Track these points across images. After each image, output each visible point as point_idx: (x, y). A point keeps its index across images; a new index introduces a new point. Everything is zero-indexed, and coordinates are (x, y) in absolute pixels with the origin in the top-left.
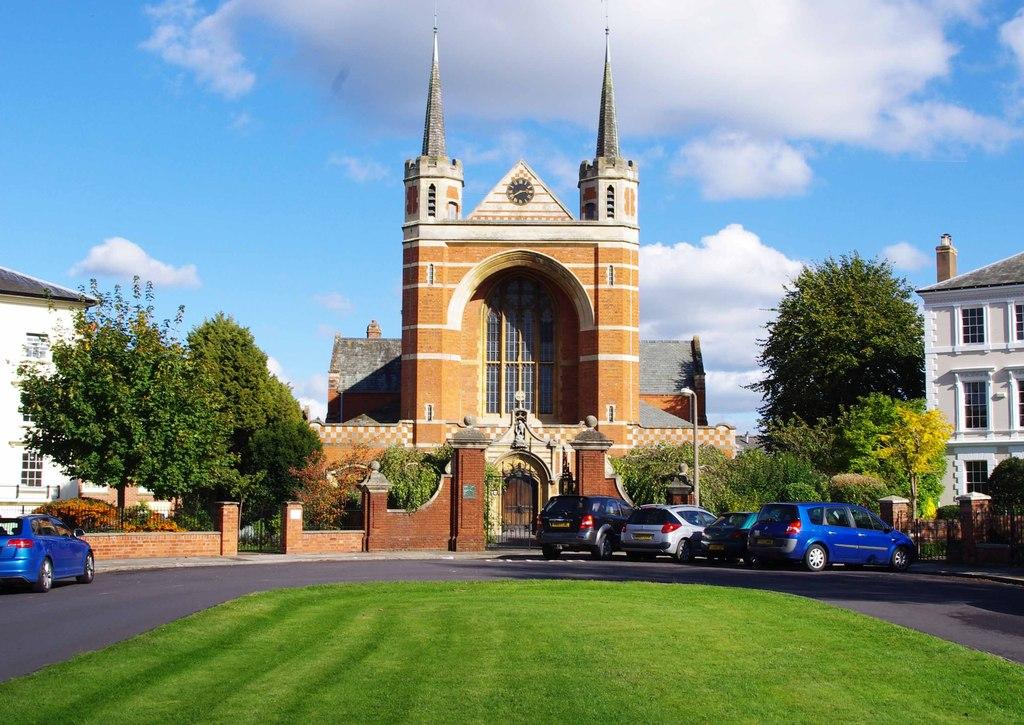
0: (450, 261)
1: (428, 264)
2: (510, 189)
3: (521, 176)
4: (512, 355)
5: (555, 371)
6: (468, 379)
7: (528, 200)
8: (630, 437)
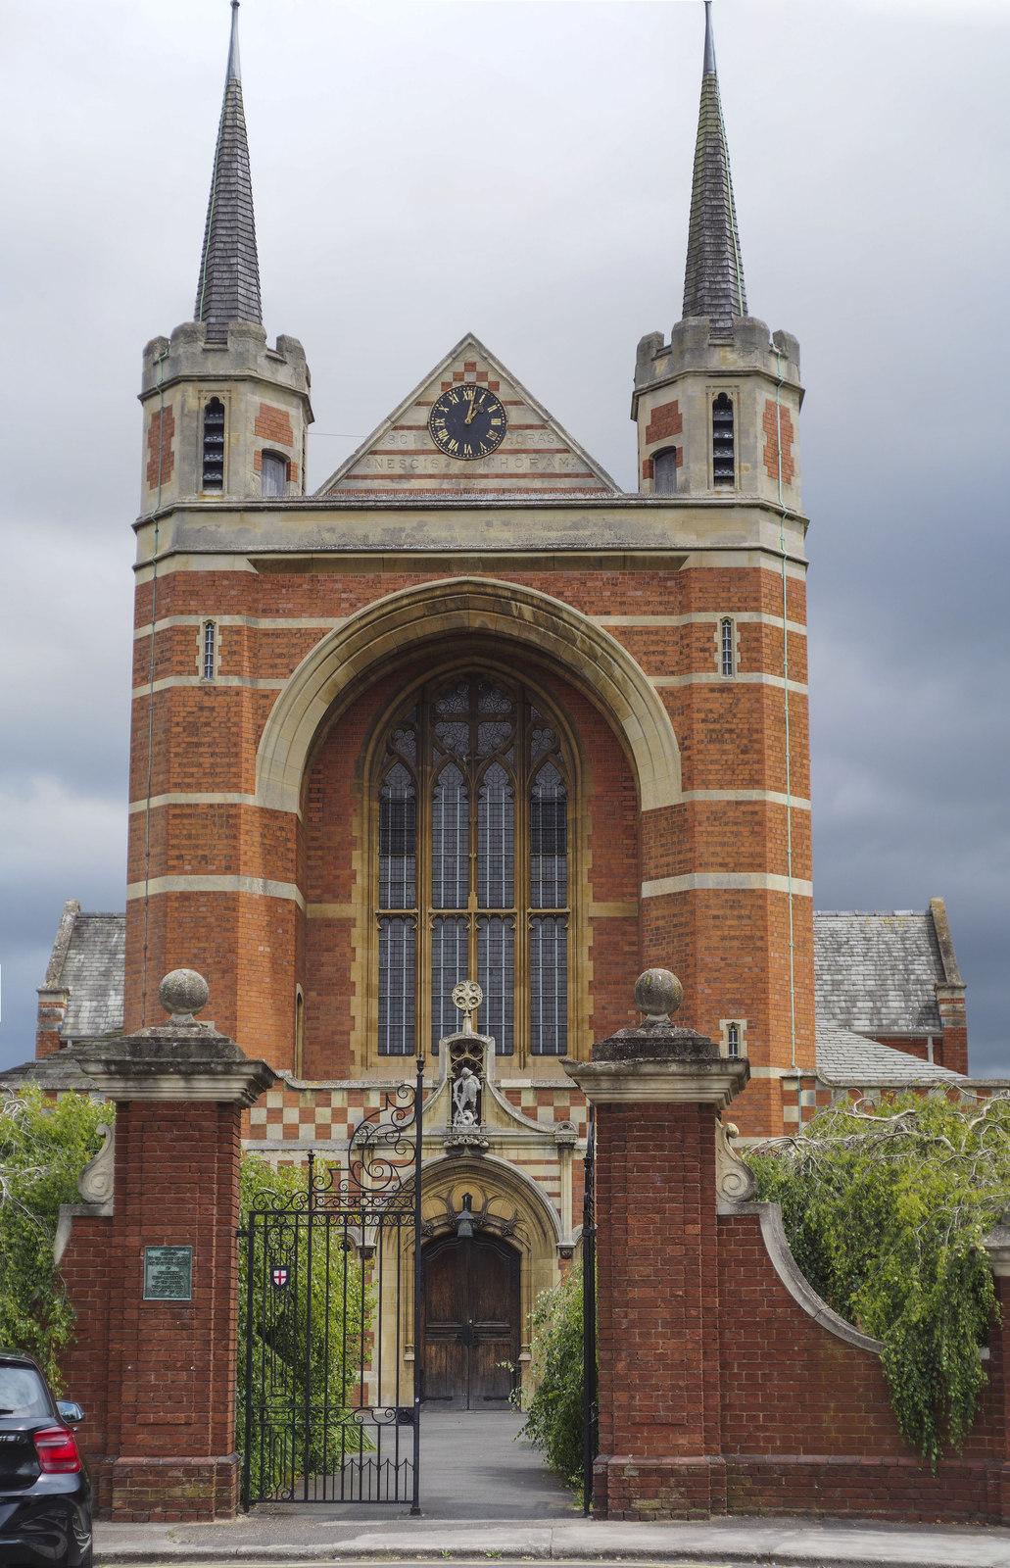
7: (489, 443)
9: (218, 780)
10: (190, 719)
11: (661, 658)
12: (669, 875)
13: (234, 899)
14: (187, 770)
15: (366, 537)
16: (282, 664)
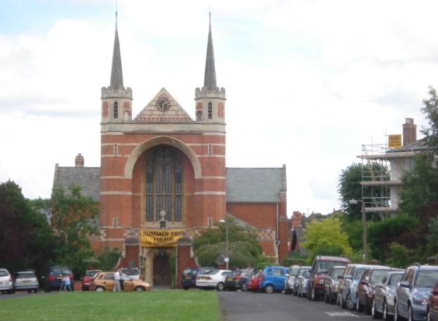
16: (129, 152)
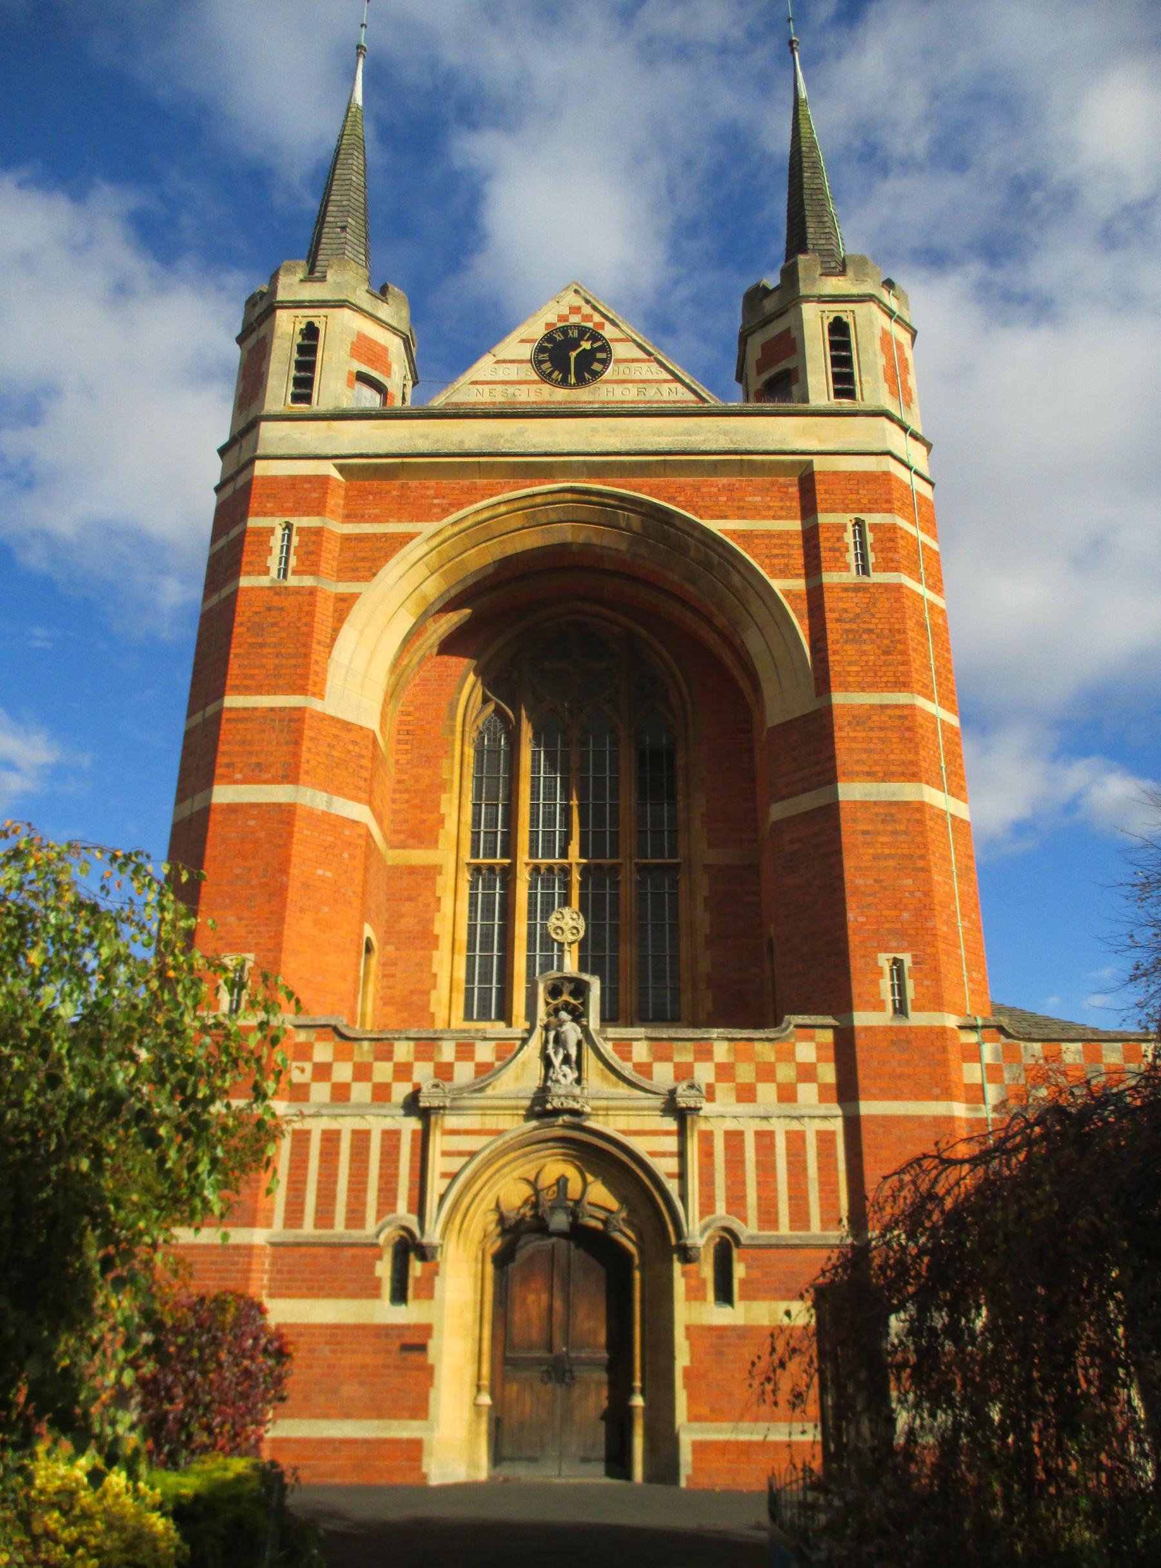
0: (349, 518)
1: (276, 523)
2: (541, 349)
3: (575, 319)
4: (549, 838)
5: (683, 886)
6: (407, 907)
8: (972, 1073)
9: (282, 682)
10: (257, 619)
11: (786, 561)
12: (805, 791)
13: (289, 811)
14: (247, 671)
15: (461, 442)
